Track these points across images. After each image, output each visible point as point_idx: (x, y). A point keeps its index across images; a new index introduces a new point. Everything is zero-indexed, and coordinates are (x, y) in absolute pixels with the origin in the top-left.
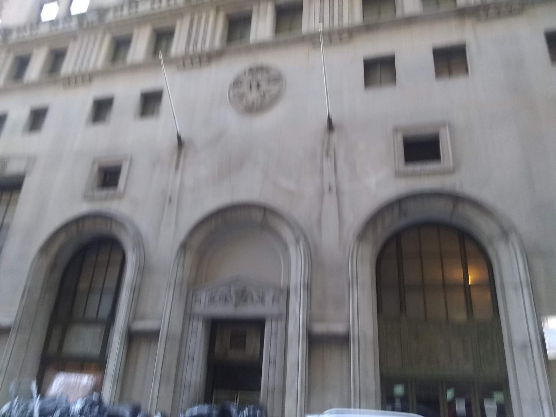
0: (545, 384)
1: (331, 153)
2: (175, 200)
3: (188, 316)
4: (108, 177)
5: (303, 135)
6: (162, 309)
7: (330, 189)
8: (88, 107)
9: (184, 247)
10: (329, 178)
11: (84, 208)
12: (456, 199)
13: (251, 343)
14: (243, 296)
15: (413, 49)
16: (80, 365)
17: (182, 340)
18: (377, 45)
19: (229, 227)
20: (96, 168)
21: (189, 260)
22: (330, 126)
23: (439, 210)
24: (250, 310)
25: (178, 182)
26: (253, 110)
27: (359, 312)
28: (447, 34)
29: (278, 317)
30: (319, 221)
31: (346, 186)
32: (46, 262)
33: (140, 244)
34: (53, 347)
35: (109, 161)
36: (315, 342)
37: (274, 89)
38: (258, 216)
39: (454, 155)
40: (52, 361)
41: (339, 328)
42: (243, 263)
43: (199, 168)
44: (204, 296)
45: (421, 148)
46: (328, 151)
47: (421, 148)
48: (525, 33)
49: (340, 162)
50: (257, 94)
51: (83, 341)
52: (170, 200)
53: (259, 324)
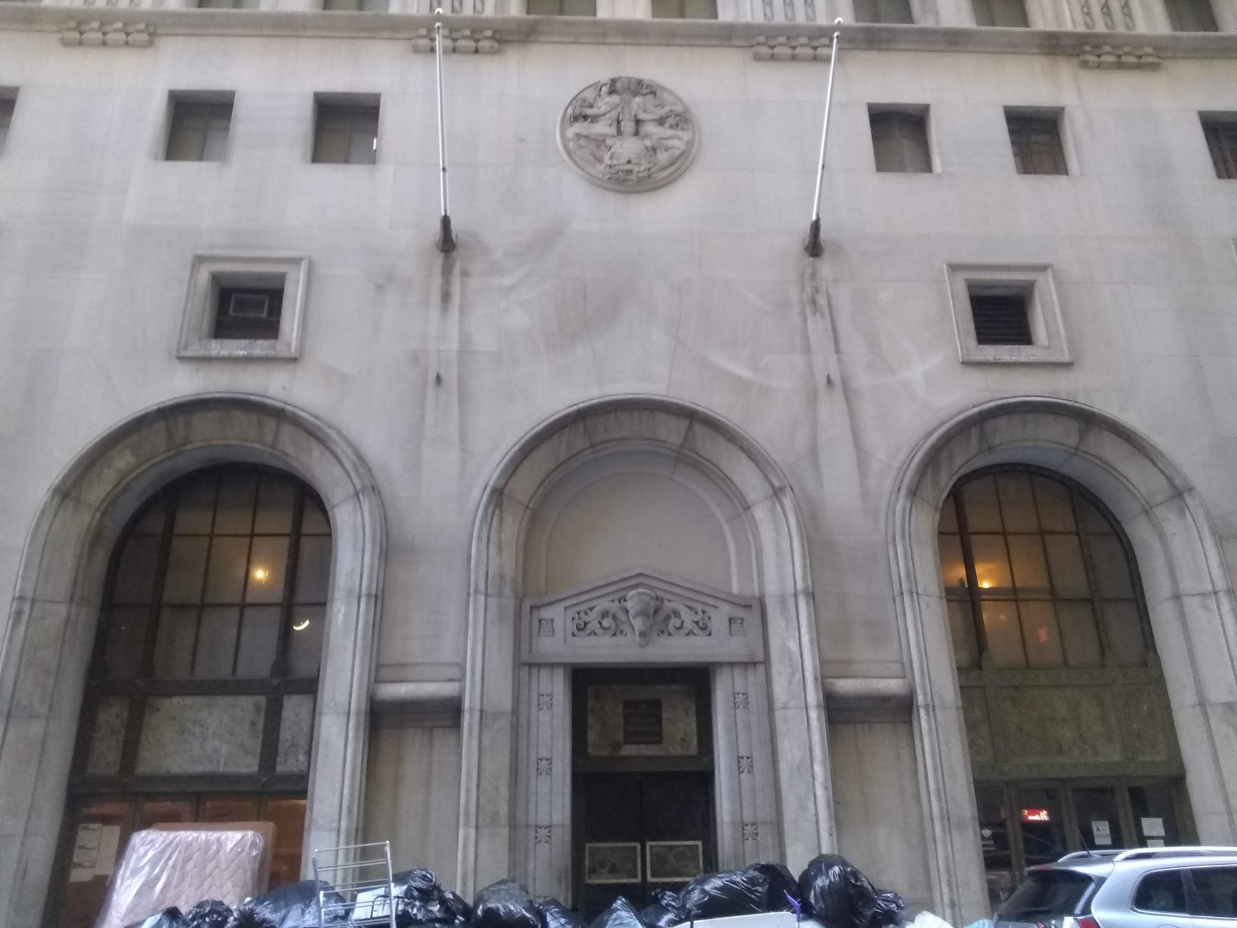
1: (822, 301)
2: (451, 377)
3: (526, 665)
4: (245, 306)
5: (778, 256)
6: (460, 647)
7: (829, 381)
8: (156, 111)
9: (498, 496)
10: (825, 362)
11: (184, 384)
12: (1087, 419)
13: (679, 723)
14: (658, 618)
15: (968, 101)
16: (206, 800)
18: (899, 81)
19: (602, 452)
20: (204, 276)
21: (512, 528)
22: (814, 247)
23: (1045, 443)
25: (454, 334)
26: (627, 182)
27: (919, 650)
28: (1034, 86)
29: (748, 664)
30: (813, 451)
31: (862, 380)
32: (79, 523)
33: (370, 488)
34: (106, 758)
35: (243, 265)
36: (842, 713)
37: (678, 141)
38: (671, 432)
39: (1069, 331)
40: (111, 791)
41: (893, 686)
42: (636, 537)
43: (503, 312)
44: (558, 616)
45: (1000, 314)
47: (245, 306)
48: (1172, 106)
49: (844, 326)
50: (633, 145)
51: (204, 736)
52: (439, 379)
53: (696, 681)
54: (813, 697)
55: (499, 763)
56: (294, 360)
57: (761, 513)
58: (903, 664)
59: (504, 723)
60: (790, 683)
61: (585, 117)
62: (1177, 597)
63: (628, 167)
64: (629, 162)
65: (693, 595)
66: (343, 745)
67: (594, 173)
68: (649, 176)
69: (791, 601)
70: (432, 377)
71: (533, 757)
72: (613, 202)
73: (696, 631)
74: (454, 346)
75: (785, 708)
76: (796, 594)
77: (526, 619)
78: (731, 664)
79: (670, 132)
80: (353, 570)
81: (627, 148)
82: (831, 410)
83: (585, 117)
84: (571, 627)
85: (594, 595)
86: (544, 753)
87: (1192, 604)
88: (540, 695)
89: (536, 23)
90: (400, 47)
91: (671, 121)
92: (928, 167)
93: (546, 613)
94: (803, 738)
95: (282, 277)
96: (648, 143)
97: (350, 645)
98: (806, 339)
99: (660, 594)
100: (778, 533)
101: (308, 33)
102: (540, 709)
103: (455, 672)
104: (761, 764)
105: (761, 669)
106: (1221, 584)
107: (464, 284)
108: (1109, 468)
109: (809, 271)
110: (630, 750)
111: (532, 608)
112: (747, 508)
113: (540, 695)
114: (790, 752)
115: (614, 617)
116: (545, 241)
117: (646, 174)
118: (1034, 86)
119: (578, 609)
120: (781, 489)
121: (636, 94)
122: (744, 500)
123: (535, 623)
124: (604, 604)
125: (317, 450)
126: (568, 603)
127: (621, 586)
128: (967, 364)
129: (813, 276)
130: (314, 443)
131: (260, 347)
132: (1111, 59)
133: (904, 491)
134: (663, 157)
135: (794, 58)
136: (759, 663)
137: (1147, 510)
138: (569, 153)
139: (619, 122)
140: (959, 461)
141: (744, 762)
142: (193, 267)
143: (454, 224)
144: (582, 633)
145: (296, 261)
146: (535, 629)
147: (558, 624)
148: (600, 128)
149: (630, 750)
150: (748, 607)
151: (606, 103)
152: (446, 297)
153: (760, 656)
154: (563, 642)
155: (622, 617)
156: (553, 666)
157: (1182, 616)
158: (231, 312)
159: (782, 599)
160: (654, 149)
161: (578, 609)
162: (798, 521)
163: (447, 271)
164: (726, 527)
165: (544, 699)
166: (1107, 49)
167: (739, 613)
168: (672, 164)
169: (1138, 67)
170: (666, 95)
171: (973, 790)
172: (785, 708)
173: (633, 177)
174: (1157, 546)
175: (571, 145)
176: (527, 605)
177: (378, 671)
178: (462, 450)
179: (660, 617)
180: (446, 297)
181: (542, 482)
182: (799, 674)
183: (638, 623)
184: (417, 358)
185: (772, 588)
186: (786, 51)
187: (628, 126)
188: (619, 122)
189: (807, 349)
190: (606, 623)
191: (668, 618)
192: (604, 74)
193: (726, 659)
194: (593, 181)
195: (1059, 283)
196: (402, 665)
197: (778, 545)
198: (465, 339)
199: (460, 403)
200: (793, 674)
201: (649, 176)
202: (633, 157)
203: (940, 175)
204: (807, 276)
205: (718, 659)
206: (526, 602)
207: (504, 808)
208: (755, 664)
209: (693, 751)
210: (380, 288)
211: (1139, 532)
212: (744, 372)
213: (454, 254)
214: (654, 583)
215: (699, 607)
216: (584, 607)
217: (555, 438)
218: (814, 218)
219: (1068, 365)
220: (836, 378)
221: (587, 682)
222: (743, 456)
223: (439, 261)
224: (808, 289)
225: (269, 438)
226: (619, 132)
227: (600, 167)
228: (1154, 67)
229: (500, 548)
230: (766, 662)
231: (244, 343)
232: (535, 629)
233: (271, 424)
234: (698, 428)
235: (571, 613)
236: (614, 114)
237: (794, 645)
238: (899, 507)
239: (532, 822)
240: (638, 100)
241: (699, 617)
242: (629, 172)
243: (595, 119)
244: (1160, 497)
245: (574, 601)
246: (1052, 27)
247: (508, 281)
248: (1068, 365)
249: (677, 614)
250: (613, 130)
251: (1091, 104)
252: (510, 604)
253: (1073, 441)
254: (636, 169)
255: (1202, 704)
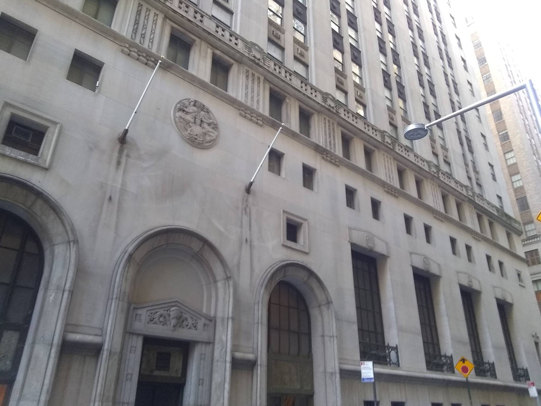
0: (51, 376)
1: (248, 210)
2: (116, 199)
3: (128, 332)
13: (176, 364)
14: (180, 321)
17: (122, 359)
19: (173, 249)
20: (7, 114)
22: (248, 190)
24: (184, 334)
26: (196, 143)
27: (257, 346)
29: (208, 343)
31: (255, 243)
33: (74, 241)
35: (32, 113)
37: (214, 134)
38: (196, 246)
41: (251, 356)
42: (173, 285)
43: (141, 178)
44: (144, 313)
45: (292, 230)
46: (246, 210)
49: (253, 222)
52: (110, 198)
53: (185, 348)
54: (229, 359)
55: (112, 376)
56: (46, 169)
57: (220, 285)
58: (253, 348)
59: (116, 357)
60: (221, 352)
61: (184, 111)
62: (323, 336)
63: (196, 137)
64: (197, 135)
65: (193, 313)
66: (46, 359)
67: (183, 133)
68: (202, 143)
69: (226, 320)
70: (107, 197)
71: (126, 373)
72: (188, 148)
73: (192, 327)
74: (119, 186)
75: (218, 361)
76: (228, 318)
77: (131, 313)
78: (202, 342)
79: (211, 130)
80: (61, 278)
81: (197, 130)
82: (245, 250)
83: (184, 111)
84: (148, 319)
85: (159, 307)
86: (130, 371)
87: (327, 339)
88: (132, 347)
89: (172, 65)
90: (116, 47)
91: (212, 126)
92: (279, 174)
93: (140, 312)
94: (223, 372)
95: (47, 128)
96: (204, 130)
97: (56, 312)
98: (242, 222)
99: (183, 311)
100: (225, 294)
101: (77, 20)
102: (131, 353)
103: (99, 332)
104: (206, 383)
105: (211, 345)
106: (335, 334)
107: (127, 160)
108: (312, 290)
109: (245, 198)
110: (156, 373)
111: (134, 308)
112: (215, 282)
113: (132, 347)
114: (217, 378)
115: (164, 317)
116: (161, 154)
117: (201, 142)
118: (314, 161)
119: (152, 312)
120: (230, 277)
121: (202, 110)
122: (215, 278)
123: (135, 315)
124: (161, 312)
125: (52, 216)
126: (148, 309)
127: (169, 305)
128: (284, 246)
129: (247, 201)
130: (52, 212)
131: (31, 158)
132: (329, 159)
133: (264, 287)
134: (208, 138)
135: (251, 120)
136: (210, 343)
137: (319, 306)
138: (175, 122)
139: (195, 118)
140: (277, 279)
141: (201, 382)
142: (3, 107)
143: (128, 135)
144: (152, 323)
145: (55, 123)
146: (134, 318)
147: (143, 317)
148: (189, 118)
149: (156, 373)
150: (211, 320)
151: (191, 109)
152: (119, 163)
153: (212, 341)
154: (145, 325)
155: (167, 318)
156: (138, 335)
157: (324, 343)
158: (13, 134)
159: (223, 319)
160: (205, 134)
161: (152, 312)
162: (233, 291)
163: (121, 152)
164: (205, 287)
165: (133, 348)
166: (329, 155)
167: (207, 322)
168: (210, 142)
169: (334, 164)
170: (211, 115)
171: (480, 335)
172: (218, 361)
173: (197, 141)
174: (319, 318)
175: (177, 119)
176: (132, 306)
177: (68, 327)
178: (116, 233)
179: (181, 320)
180: (119, 163)
181: (146, 255)
182: (225, 349)
183: (173, 322)
184: (102, 186)
185: (219, 314)
186: (249, 116)
187: (198, 122)
188: (195, 118)
189: (241, 227)
190: (161, 319)
191: (183, 321)
192: (193, 98)
193: (201, 340)
194: (183, 137)
195: (308, 226)
196: (76, 325)
197: (224, 299)
198: (123, 184)
199: (118, 211)
200: (222, 349)
201: (202, 143)
202: (198, 133)
203: (284, 179)
204: (245, 200)
205: (198, 340)
206: (132, 305)
207: (111, 394)
208: (210, 343)
209: (179, 375)
210: (91, 149)
211: (314, 312)
212: (222, 229)
213: (125, 146)
214: (182, 306)
215: (195, 318)
216: (153, 311)
217: (155, 237)
218: (252, 181)
219: (307, 254)
220: (248, 239)
221: (150, 342)
222: (219, 261)
223: (118, 146)
224: (245, 205)
225: (29, 203)
226: (195, 122)
227: (187, 133)
228: (338, 166)
229: (126, 280)
230: (213, 343)
231: (23, 153)
232: (134, 318)
233: (32, 197)
234: (206, 247)
235: (149, 312)
236: (194, 114)
237: (225, 336)
238: (262, 292)
239: (122, 401)
240: (203, 113)
241: (194, 322)
242: (196, 139)
243: (187, 113)
244: (323, 303)
245: (150, 308)
246: (317, 143)
247: (145, 165)
248: (307, 254)
249: (187, 319)
250: (192, 120)
251: (324, 172)
252: (126, 305)
253: (306, 279)
254: (198, 139)
255: (325, 371)
